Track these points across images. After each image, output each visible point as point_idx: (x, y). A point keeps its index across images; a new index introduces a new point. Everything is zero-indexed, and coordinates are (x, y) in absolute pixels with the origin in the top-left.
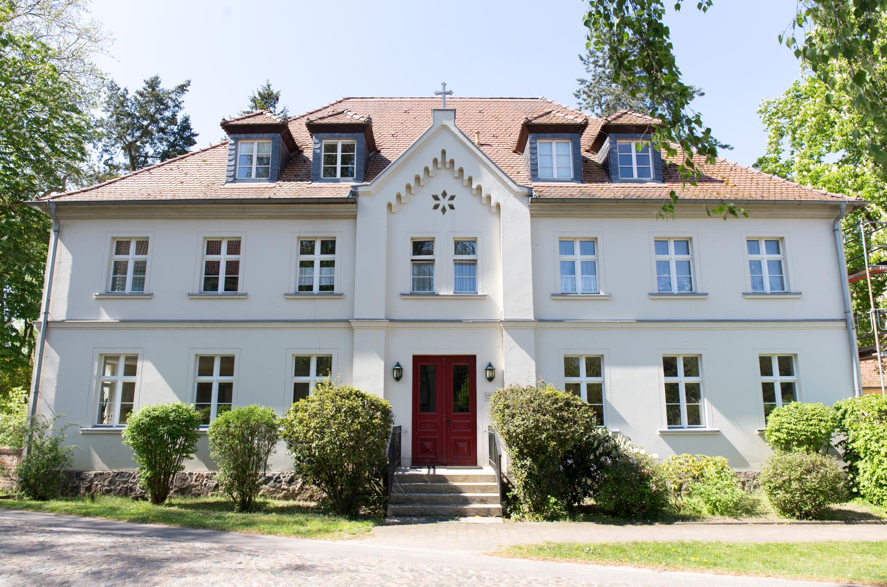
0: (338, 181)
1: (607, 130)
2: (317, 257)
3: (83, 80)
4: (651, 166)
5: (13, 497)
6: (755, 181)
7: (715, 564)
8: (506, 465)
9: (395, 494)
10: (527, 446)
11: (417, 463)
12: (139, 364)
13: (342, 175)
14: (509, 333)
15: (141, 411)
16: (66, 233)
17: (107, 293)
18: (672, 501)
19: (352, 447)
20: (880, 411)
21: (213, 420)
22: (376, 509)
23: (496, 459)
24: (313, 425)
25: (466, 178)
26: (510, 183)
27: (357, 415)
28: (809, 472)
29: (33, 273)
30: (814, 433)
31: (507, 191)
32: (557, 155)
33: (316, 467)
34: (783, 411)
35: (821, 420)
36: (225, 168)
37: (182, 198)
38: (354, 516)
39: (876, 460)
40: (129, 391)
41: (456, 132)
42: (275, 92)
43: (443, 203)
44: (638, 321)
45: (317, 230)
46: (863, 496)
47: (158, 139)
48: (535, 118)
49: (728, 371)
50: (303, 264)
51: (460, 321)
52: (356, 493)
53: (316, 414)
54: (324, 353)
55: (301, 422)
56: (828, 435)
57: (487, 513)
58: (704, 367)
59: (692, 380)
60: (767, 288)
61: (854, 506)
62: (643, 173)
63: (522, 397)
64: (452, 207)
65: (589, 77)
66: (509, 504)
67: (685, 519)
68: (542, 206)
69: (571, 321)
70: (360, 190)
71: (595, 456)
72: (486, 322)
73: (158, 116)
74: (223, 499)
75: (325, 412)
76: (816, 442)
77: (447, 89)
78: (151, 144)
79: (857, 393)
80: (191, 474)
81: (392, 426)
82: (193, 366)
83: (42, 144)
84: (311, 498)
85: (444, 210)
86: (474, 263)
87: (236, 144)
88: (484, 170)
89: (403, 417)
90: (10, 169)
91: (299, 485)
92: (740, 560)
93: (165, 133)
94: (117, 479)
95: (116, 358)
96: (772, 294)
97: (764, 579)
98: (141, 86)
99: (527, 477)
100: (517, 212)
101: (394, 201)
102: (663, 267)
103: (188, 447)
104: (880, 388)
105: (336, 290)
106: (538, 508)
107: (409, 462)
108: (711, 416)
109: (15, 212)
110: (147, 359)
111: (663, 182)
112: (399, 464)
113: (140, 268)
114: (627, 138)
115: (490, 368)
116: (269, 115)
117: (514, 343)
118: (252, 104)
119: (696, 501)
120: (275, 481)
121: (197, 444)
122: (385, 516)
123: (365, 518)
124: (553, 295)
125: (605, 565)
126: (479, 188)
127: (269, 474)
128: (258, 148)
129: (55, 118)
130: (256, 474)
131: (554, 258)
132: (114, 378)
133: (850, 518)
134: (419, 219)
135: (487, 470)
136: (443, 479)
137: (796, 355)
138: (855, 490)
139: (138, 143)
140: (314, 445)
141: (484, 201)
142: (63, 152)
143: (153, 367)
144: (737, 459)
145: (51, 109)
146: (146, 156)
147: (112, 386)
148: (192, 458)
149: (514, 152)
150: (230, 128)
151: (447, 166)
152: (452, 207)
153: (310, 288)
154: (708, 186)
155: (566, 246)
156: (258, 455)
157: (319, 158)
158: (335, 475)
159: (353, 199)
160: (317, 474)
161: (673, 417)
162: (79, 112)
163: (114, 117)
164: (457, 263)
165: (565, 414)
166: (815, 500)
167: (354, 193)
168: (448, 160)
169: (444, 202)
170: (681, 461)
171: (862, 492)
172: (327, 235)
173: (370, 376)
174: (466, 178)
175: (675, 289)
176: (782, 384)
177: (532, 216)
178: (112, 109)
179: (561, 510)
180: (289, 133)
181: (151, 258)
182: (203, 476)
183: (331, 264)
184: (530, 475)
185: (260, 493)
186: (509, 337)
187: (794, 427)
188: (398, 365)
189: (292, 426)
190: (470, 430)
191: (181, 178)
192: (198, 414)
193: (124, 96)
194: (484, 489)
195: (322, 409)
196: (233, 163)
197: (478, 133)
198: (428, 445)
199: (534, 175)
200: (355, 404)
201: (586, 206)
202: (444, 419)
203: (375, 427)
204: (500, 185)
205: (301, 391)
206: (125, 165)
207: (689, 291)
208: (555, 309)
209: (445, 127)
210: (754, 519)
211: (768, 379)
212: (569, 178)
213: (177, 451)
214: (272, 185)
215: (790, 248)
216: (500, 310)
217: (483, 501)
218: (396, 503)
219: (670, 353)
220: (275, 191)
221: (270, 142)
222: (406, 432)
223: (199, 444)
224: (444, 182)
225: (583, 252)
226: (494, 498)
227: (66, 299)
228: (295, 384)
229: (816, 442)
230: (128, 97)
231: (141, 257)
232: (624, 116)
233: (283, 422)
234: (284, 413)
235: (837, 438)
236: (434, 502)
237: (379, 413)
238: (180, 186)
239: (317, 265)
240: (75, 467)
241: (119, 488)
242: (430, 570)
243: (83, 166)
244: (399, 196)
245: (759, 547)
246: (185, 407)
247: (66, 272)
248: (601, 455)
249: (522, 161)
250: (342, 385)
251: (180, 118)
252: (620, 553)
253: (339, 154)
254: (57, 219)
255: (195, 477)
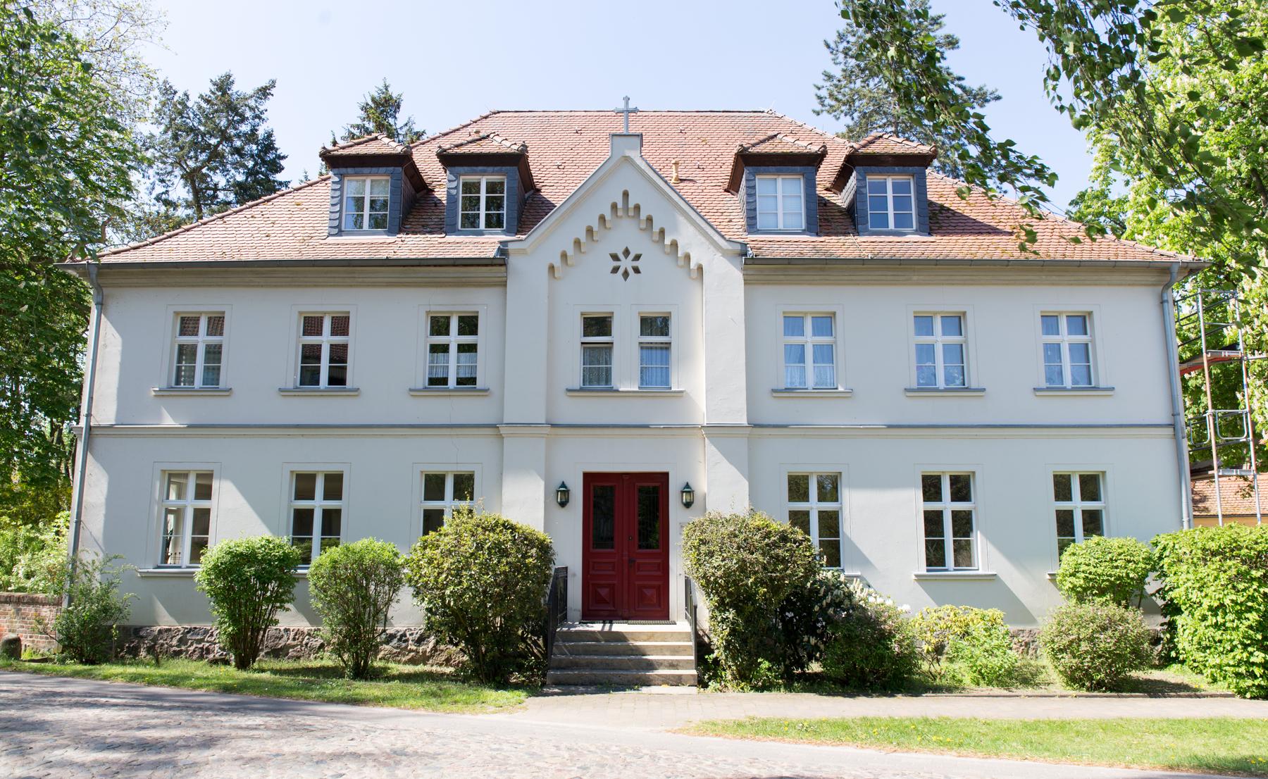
0: (481, 233)
1: (853, 162)
2: (454, 338)
3: (125, 82)
4: (914, 212)
5: (51, 660)
6: (1057, 232)
7: (961, 745)
8: (705, 623)
9: (557, 657)
10: (730, 595)
11: (588, 617)
12: (215, 485)
13: (488, 225)
14: (712, 443)
15: (219, 546)
16: (112, 306)
17: (170, 388)
18: (925, 666)
19: (499, 594)
20: (1204, 550)
21: (316, 559)
22: (533, 675)
23: (692, 610)
24: (446, 565)
25: (656, 229)
26: (717, 238)
27: (504, 553)
28: (1104, 629)
29: (62, 355)
30: (1119, 578)
31: (712, 248)
32: (783, 197)
33: (454, 621)
34: (1083, 545)
35: (1129, 561)
36: (327, 216)
37: (269, 258)
38: (503, 685)
39: (1197, 614)
40: (202, 518)
41: (643, 166)
42: (394, 96)
43: (625, 265)
44: (890, 427)
45: (453, 302)
46: (1183, 662)
47: (232, 164)
48: (753, 145)
49: (1013, 494)
50: (435, 349)
51: (647, 427)
52: (504, 655)
53: (450, 552)
54: (464, 469)
55: (430, 561)
56: (1141, 580)
57: (678, 681)
58: (978, 489)
59: (961, 506)
60: (1068, 383)
61: (1171, 674)
62: (902, 221)
63: (723, 530)
64: (637, 270)
65: (837, 72)
66: (707, 669)
67: (937, 690)
68: (759, 269)
69: (798, 426)
70: (511, 247)
71: (821, 607)
72: (683, 427)
73: (232, 132)
74: (330, 664)
75: (462, 549)
76: (1125, 591)
77: (631, 106)
78: (223, 171)
79: (1186, 524)
80: (287, 630)
81: (553, 567)
82: (287, 487)
83: (71, 176)
84: (448, 661)
85: (626, 274)
86: (666, 347)
87: (341, 182)
88: (681, 219)
89: (569, 553)
90: (29, 211)
91: (431, 645)
92: (994, 741)
93: (242, 156)
94: (188, 636)
95: (185, 475)
96: (1073, 389)
97: (1019, 762)
98: (207, 89)
99: (729, 634)
100: (726, 278)
101: (557, 262)
102: (926, 352)
103: (282, 594)
104: (1255, 515)
105: (479, 384)
106: (745, 676)
107: (578, 615)
108: (986, 555)
109: (37, 272)
110: (227, 478)
111: (930, 234)
112: (565, 618)
113: (214, 353)
114: (880, 173)
115: (687, 489)
116: (386, 140)
117: (719, 456)
118: (363, 114)
119: (962, 670)
120: (400, 640)
121: (294, 591)
122: (544, 685)
123: (517, 687)
124: (774, 391)
125: (819, 745)
126: (674, 245)
127: (390, 631)
128: (373, 187)
129: (88, 139)
130: (374, 630)
131: (775, 339)
132: (181, 503)
133: (1156, 690)
134: (594, 289)
135: (684, 626)
136: (620, 637)
137: (1104, 473)
138: (1173, 654)
139: (204, 171)
140: (448, 592)
141: (681, 262)
142: (100, 187)
143: (234, 488)
144: (1018, 611)
145: (82, 127)
146: (216, 189)
147: (179, 513)
148: (288, 610)
149: (726, 191)
150: (333, 160)
151: (632, 213)
152: (637, 270)
153: (444, 381)
154: (986, 239)
155: (793, 323)
156: (375, 605)
157: (456, 201)
158: (477, 632)
159: (501, 259)
160: (453, 630)
161: (935, 556)
162: (121, 131)
163: (170, 134)
164: (643, 346)
165: (780, 552)
166: (1110, 666)
167: (503, 251)
168: (631, 205)
169: (626, 264)
170: (941, 614)
171: (1181, 657)
172: (467, 309)
173: (527, 503)
174: (656, 229)
175: (941, 383)
176: (1084, 512)
177: (747, 282)
178: (166, 121)
179: (776, 677)
180: (413, 165)
181: (228, 340)
182: (303, 633)
183: (472, 348)
184: (733, 632)
185: (380, 656)
186: (713, 448)
187: (1093, 570)
188: (563, 485)
189: (420, 567)
190: (659, 573)
191: (268, 230)
192: (297, 551)
193: (183, 103)
194: (675, 650)
195: (458, 545)
196: (337, 208)
197: (676, 164)
198: (604, 592)
199: (751, 225)
200: (503, 538)
201: (821, 269)
202: (626, 558)
203: (528, 569)
204: (703, 239)
205: (432, 521)
206: (186, 201)
207: (961, 387)
208: (777, 410)
209: (627, 159)
210: (1030, 691)
211: (1064, 505)
212: (799, 229)
213: (268, 600)
214: (391, 239)
215: (1099, 325)
216: (702, 413)
217: (672, 665)
218: (558, 668)
219: (932, 470)
220: (395, 247)
221: (391, 178)
222: (574, 575)
223: (297, 590)
224: (626, 235)
225: (816, 332)
226: (687, 661)
227: (115, 397)
228: (425, 511)
229: (1125, 591)
230: (190, 104)
231: (214, 340)
232: (878, 142)
233: (407, 562)
234: (403, 546)
235: (1151, 587)
236: (609, 666)
237: (534, 551)
238: (265, 241)
239: (453, 349)
240: (133, 621)
241: (192, 648)
242: (593, 749)
243: (128, 205)
244: (564, 256)
245: (1026, 725)
246: (277, 541)
247: (111, 360)
248: (829, 605)
249: (735, 204)
250: (485, 513)
251: (261, 133)
252: (843, 730)
253: (483, 195)
254: (99, 288)
255: (292, 634)
